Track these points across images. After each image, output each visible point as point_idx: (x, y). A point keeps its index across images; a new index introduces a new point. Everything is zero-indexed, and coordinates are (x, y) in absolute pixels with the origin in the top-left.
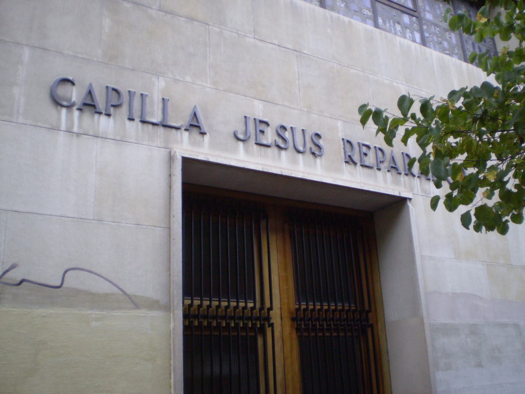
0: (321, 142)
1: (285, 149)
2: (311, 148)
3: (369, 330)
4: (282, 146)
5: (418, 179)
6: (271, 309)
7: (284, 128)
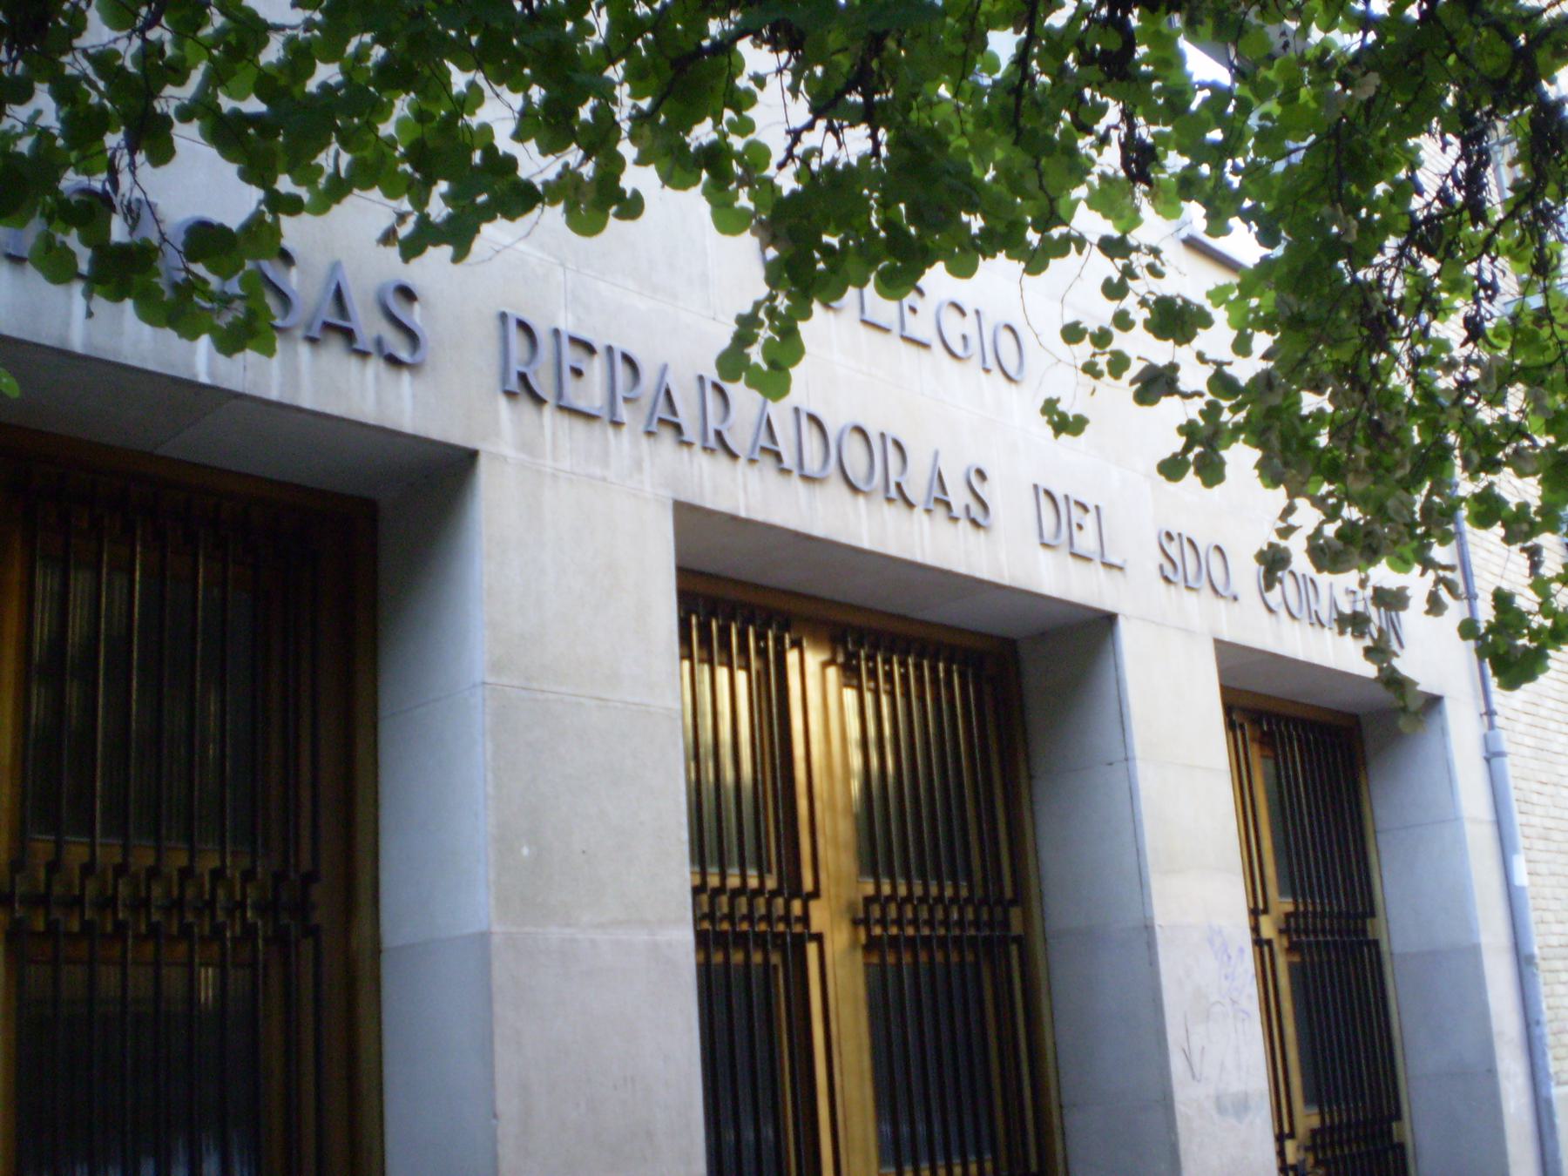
0: (415, 316)
1: (413, 367)
2: (967, 508)
3: (812, 949)
4: (404, 355)
5: (925, 517)
6: (310, 878)
7: (1169, 536)
